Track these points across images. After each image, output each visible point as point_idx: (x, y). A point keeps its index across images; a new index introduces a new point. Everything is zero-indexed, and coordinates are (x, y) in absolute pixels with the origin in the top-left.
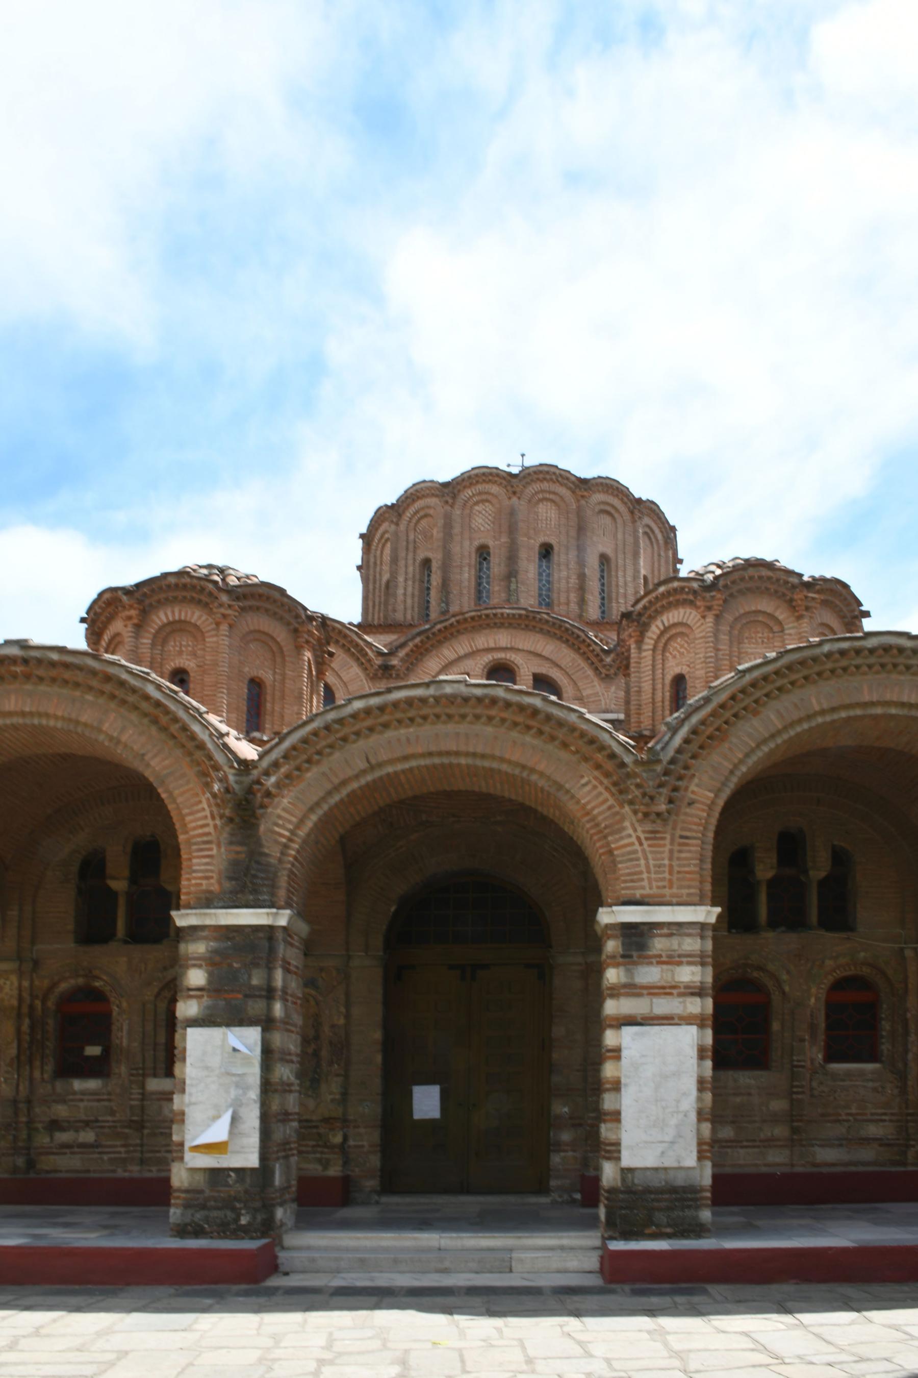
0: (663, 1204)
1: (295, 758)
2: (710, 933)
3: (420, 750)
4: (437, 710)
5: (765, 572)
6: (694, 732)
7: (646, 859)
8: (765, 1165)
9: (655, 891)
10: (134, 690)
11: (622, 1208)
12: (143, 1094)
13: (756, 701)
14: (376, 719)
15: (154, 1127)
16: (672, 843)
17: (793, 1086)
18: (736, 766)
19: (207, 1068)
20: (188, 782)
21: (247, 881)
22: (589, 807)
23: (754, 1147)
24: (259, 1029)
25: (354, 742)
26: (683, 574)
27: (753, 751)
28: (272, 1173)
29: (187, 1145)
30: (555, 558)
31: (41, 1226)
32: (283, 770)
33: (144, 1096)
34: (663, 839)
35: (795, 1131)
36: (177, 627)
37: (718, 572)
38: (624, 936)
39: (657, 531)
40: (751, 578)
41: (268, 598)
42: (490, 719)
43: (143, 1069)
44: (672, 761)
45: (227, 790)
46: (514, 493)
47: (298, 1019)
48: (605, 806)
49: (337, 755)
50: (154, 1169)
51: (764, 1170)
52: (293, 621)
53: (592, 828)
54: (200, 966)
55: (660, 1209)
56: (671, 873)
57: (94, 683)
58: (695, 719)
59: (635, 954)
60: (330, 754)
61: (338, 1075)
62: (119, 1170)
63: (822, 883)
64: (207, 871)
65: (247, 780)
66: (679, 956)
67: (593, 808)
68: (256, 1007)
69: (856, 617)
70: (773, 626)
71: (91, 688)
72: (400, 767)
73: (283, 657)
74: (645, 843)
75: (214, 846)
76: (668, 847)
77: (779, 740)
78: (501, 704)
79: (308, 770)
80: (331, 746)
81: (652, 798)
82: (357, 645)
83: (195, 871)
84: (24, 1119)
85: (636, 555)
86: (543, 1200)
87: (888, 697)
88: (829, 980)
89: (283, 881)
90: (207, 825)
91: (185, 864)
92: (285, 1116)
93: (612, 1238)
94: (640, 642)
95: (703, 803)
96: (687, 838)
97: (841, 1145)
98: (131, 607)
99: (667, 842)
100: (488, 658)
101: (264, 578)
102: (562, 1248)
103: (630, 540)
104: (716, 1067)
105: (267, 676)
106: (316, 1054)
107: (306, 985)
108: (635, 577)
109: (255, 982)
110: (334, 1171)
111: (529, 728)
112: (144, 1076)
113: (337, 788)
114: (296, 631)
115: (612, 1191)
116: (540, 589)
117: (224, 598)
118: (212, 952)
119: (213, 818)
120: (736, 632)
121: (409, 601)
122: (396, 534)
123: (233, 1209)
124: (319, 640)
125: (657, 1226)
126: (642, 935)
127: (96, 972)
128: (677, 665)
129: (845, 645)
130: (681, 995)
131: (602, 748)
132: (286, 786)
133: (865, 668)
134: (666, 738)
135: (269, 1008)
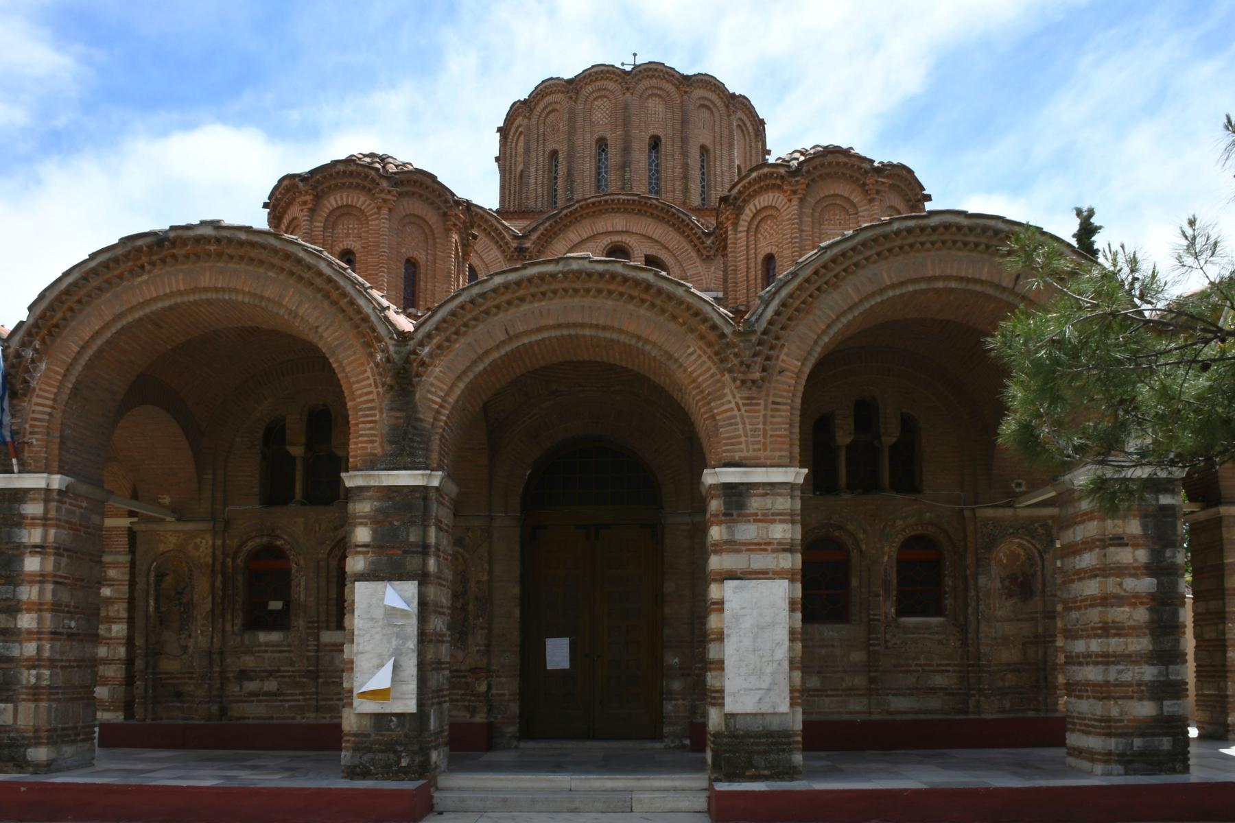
0: (762, 748)
1: (446, 330)
2: (798, 493)
3: (550, 322)
4: (565, 285)
5: (842, 159)
6: (784, 304)
7: (744, 423)
8: (847, 713)
9: (751, 454)
10: (309, 267)
11: (725, 751)
12: (318, 646)
13: (836, 276)
14: (514, 294)
15: (327, 675)
16: (766, 409)
17: (870, 639)
18: (819, 337)
19: (372, 619)
20: (355, 353)
21: (405, 446)
22: (694, 375)
23: (837, 696)
24: (416, 582)
25: (495, 315)
26: (771, 159)
27: (834, 322)
28: (428, 718)
29: (356, 692)
30: (663, 149)
31: (231, 769)
32: (435, 341)
33: (319, 647)
34: (758, 404)
35: (872, 680)
36: (345, 211)
37: (802, 158)
38: (725, 495)
39: (749, 124)
40: (830, 164)
41: (421, 184)
42: (610, 292)
43: (318, 622)
44: (765, 332)
45: (388, 360)
46: (628, 89)
47: (448, 574)
48: (708, 375)
49: (481, 327)
50: (328, 716)
51: (847, 717)
52: (442, 206)
53: (697, 394)
54: (365, 525)
55: (758, 753)
56: (765, 437)
57: (276, 261)
58: (784, 293)
59: (735, 513)
60: (475, 326)
61: (482, 628)
62: (299, 717)
63: (893, 448)
64: (372, 435)
65: (405, 350)
66: (773, 514)
67: (698, 376)
68: (413, 562)
69: (919, 200)
70: (849, 208)
71: (273, 266)
72: (534, 338)
73: (434, 239)
74: (743, 409)
75: (377, 412)
76: (763, 412)
77: (856, 313)
78: (619, 279)
79: (456, 341)
80: (475, 319)
81: (748, 366)
82: (496, 229)
83: (362, 435)
84: (218, 669)
85: (731, 146)
86: (658, 745)
87: (948, 272)
88: (899, 539)
89: (435, 444)
90: (371, 393)
91: (352, 429)
92: (438, 665)
93: (717, 780)
94: (736, 224)
95: (792, 372)
96: (778, 403)
97: (912, 695)
98: (306, 192)
99: (762, 407)
100: (607, 241)
101: (418, 165)
102: (675, 789)
103: (726, 132)
104: (804, 620)
105: (421, 257)
106: (464, 609)
107: (455, 544)
108: (730, 167)
109: (412, 539)
110: (480, 718)
111: (643, 301)
112: (319, 628)
113: (480, 358)
114: (445, 214)
115: (717, 735)
116: (650, 178)
117: (385, 184)
118: (376, 511)
119: (376, 386)
120: (817, 215)
121: (540, 190)
122: (528, 127)
123: (395, 752)
124: (464, 223)
125: (757, 768)
126: (740, 495)
127: (278, 532)
128: (768, 245)
129: (911, 223)
130: (774, 551)
131: (705, 320)
132: (438, 356)
133: (928, 245)
134: (760, 310)
135: (425, 564)
